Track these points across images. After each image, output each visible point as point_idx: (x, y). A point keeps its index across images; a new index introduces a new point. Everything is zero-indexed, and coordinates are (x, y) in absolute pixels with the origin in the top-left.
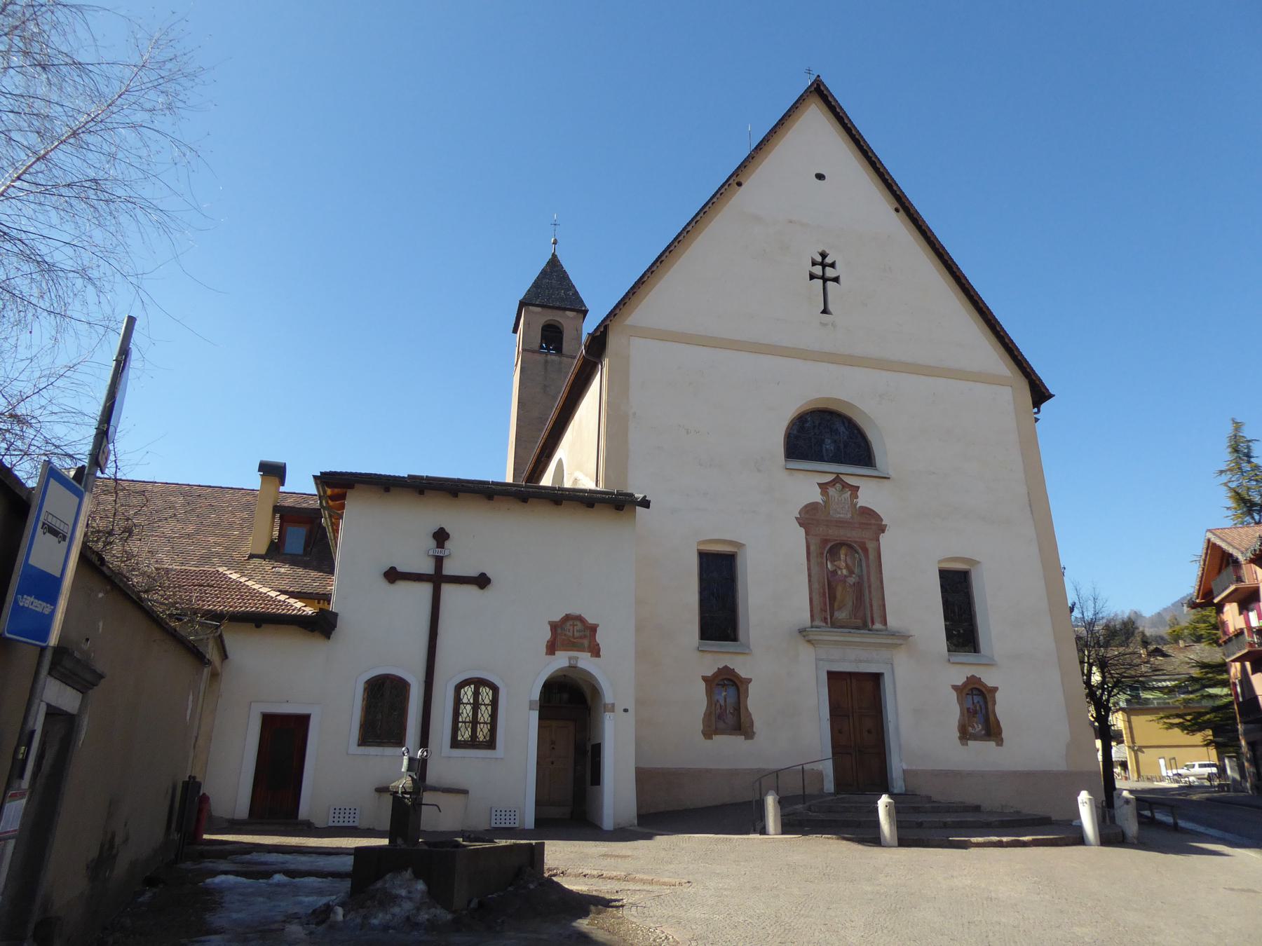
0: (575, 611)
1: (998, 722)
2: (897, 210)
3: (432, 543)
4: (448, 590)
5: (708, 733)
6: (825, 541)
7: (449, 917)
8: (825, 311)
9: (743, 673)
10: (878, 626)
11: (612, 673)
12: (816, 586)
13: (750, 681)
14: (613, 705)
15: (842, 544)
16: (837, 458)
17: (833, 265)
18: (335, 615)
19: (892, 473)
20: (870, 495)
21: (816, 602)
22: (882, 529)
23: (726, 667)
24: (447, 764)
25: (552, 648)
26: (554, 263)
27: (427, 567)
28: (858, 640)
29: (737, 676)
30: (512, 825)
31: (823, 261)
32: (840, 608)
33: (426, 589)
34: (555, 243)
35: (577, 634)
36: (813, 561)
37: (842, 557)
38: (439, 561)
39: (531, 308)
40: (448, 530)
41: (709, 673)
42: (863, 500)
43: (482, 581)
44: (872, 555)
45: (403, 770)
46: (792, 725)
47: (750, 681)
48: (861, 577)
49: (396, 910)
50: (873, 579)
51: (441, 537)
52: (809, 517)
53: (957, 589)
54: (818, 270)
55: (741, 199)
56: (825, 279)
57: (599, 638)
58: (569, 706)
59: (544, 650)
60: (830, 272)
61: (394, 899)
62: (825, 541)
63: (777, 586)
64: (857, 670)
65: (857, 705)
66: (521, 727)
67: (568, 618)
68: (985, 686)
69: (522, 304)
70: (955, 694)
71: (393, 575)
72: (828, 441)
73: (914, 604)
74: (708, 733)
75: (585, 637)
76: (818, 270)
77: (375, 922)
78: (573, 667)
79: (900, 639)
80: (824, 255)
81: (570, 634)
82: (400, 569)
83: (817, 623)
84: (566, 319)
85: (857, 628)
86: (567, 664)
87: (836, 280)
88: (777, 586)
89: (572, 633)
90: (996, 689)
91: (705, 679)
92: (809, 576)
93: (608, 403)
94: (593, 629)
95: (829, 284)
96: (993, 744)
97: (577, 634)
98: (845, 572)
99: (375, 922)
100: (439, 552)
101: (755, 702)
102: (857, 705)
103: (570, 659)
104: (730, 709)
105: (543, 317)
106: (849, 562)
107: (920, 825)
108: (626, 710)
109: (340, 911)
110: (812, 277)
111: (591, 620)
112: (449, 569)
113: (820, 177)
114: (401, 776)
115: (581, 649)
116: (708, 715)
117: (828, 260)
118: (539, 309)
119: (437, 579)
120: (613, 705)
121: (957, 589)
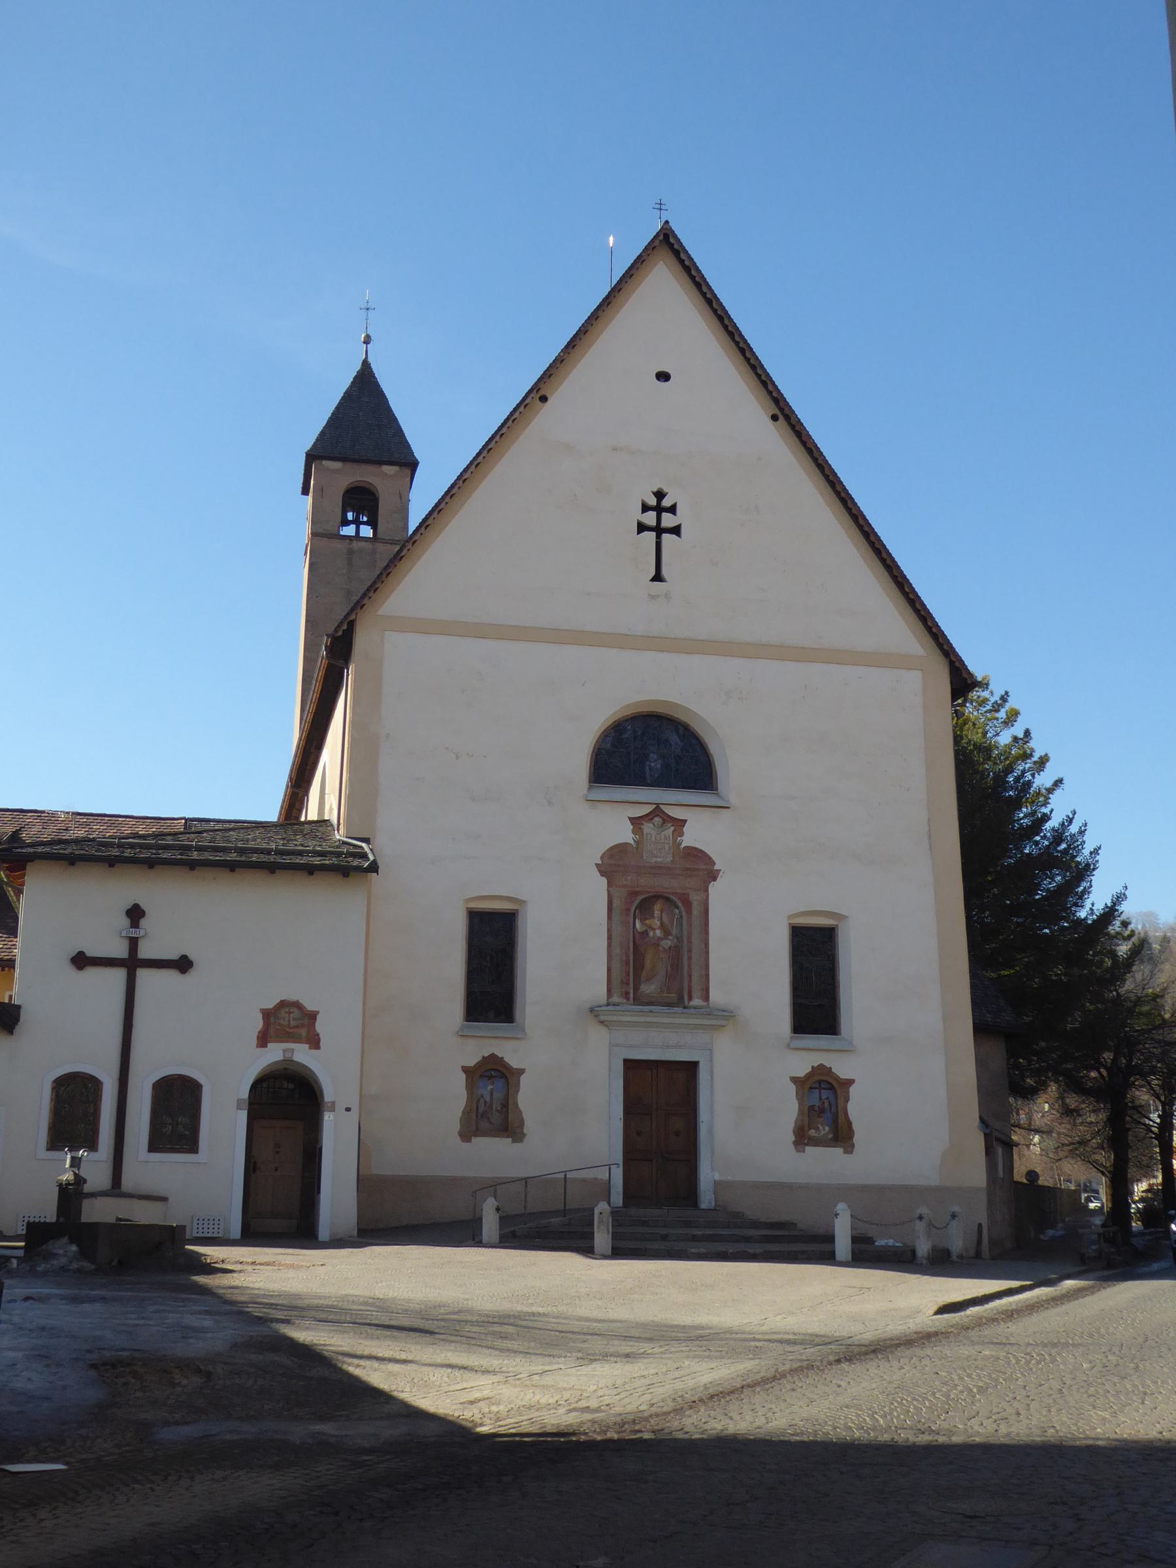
0: (293, 997)
1: (850, 1124)
2: (774, 418)
3: (125, 922)
4: (144, 976)
5: (465, 1136)
6: (633, 894)
7: (93, 1267)
8: (658, 577)
9: (514, 1062)
10: (697, 1002)
11: (333, 1067)
12: (617, 950)
13: (521, 1072)
14: (333, 1103)
15: (657, 897)
16: (664, 781)
17: (672, 510)
18: (19, 1007)
19: (733, 799)
20: (702, 829)
21: (614, 974)
22: (713, 876)
23: (493, 1056)
24: (148, 1168)
25: (263, 1040)
26: (365, 381)
27: (120, 950)
28: (666, 1020)
29: (507, 1067)
30: (216, 1235)
31: (659, 504)
32: (648, 980)
33: (118, 976)
34: (367, 340)
35: (293, 1023)
36: (616, 918)
37: (657, 913)
38: (134, 943)
39: (326, 463)
40: (144, 907)
41: (472, 1062)
42: (689, 839)
43: (183, 965)
44: (696, 911)
45: (67, 1166)
46: (576, 1126)
47: (521, 1072)
48: (679, 939)
49: (55, 1262)
50: (696, 941)
51: (135, 914)
52: (614, 864)
53: (814, 956)
54: (650, 518)
55: (544, 418)
56: (659, 530)
57: (319, 1027)
58: (287, 1102)
59: (255, 1042)
60: (668, 520)
61: (55, 1256)
62: (633, 894)
63: (566, 955)
64: (663, 1058)
65: (662, 1102)
66: (225, 1125)
67: (283, 1004)
68: (837, 1078)
69: (312, 457)
70: (793, 1087)
71: (81, 961)
72: (653, 756)
73: (748, 968)
74: (465, 1136)
75: (303, 1026)
76: (650, 518)
77: (39, 1269)
78: (288, 1061)
79: (725, 1017)
80: (660, 495)
81: (286, 1023)
82: (90, 953)
83: (615, 999)
84: (381, 478)
85: (669, 1005)
86: (281, 1058)
87: (676, 530)
88: (566, 955)
89: (288, 1021)
90: (850, 1082)
91: (465, 1070)
92: (610, 938)
93: (352, 722)
94: (313, 1016)
95: (665, 536)
96: (840, 1150)
97: (293, 1023)
98: (658, 933)
99: (39, 1269)
100: (133, 933)
101: (527, 1098)
102: (662, 1102)
103: (285, 1051)
104: (497, 1106)
105: (344, 476)
106: (665, 919)
107: (664, 1238)
108: (348, 1109)
109: (15, 1262)
110: (642, 528)
111: (310, 1006)
112: (146, 951)
113: (663, 377)
114: (65, 1171)
115: (297, 1039)
116: (466, 1113)
117: (666, 503)
118: (337, 465)
119: (132, 963)
120: (333, 1103)
121: (814, 956)
